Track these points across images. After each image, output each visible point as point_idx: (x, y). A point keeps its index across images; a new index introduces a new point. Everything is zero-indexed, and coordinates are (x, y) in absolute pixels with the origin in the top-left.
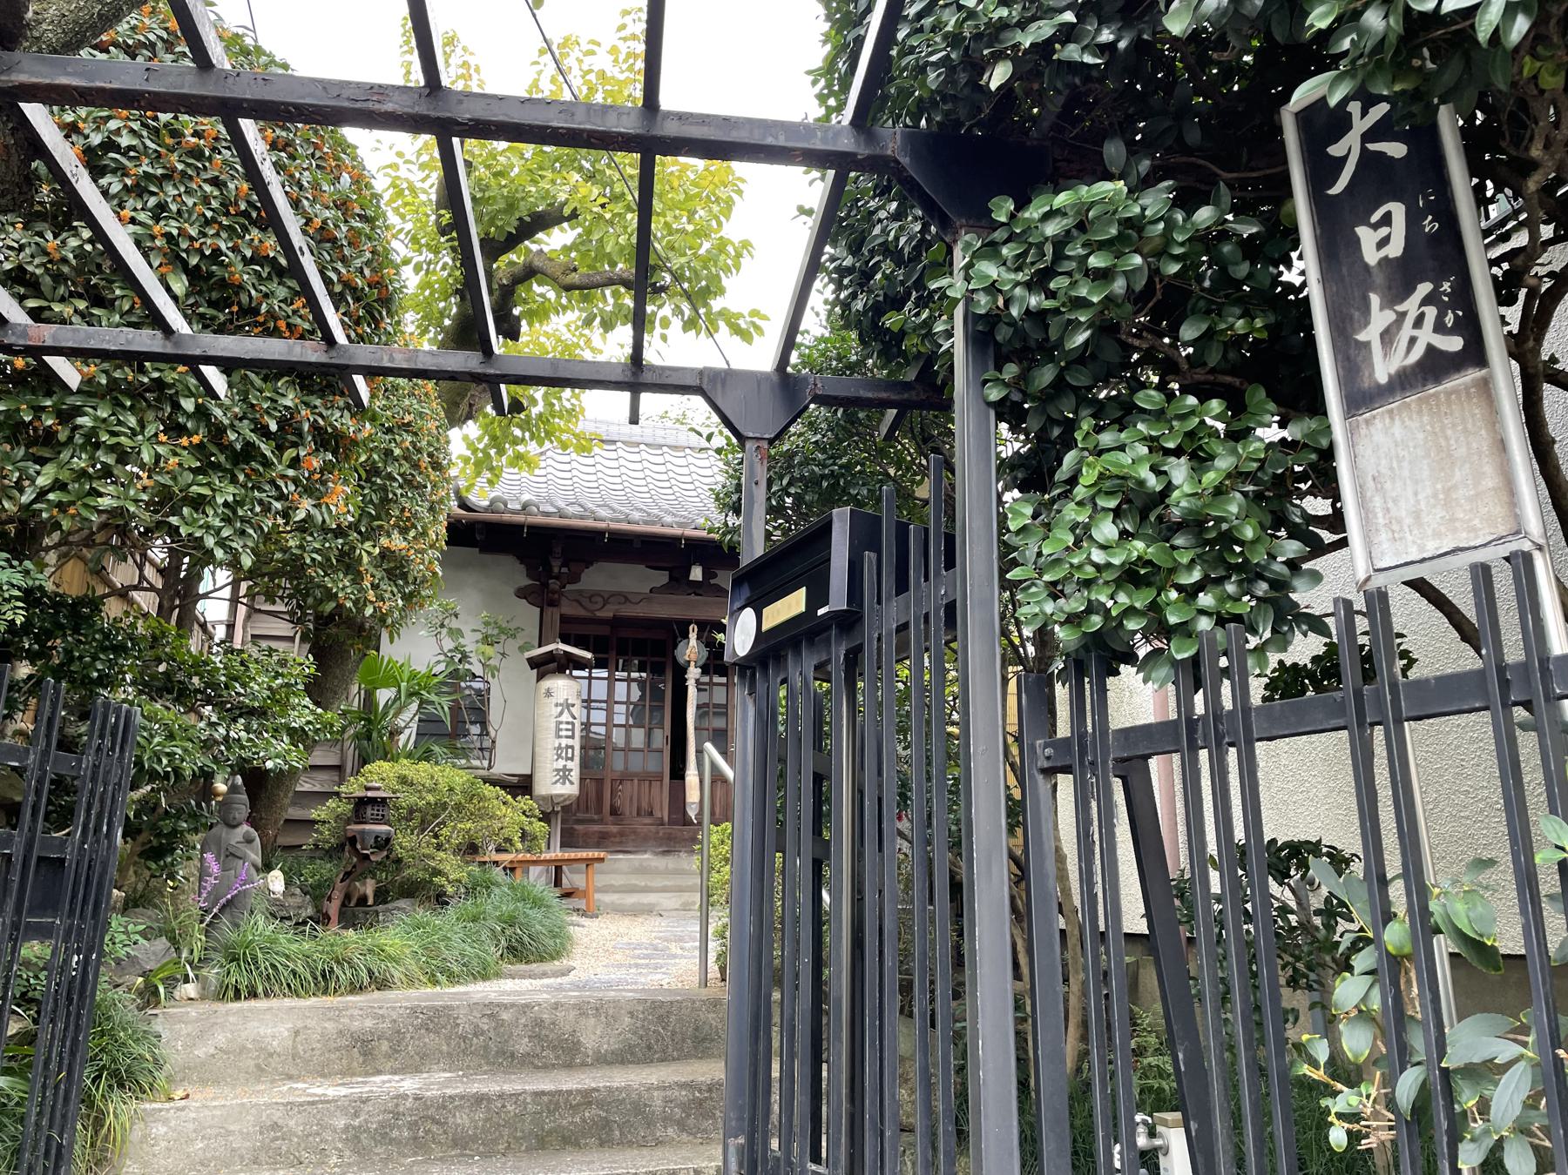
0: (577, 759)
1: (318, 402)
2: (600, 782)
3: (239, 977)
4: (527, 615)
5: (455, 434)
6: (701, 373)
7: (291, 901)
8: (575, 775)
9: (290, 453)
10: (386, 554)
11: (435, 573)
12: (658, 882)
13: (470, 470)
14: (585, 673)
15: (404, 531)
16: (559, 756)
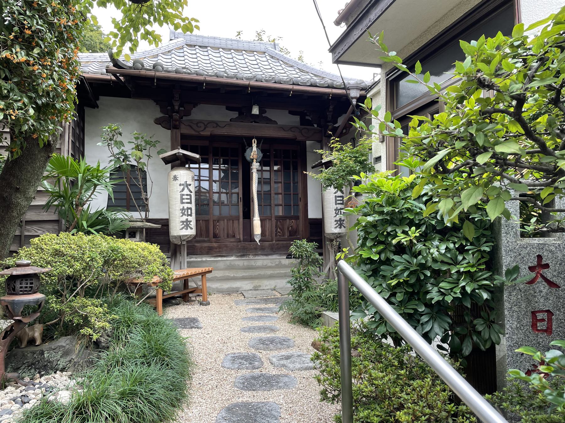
0: (194, 215)
2: (207, 221)
4: (164, 135)
8: (193, 224)
12: (240, 274)
14: (197, 166)
16: (183, 214)
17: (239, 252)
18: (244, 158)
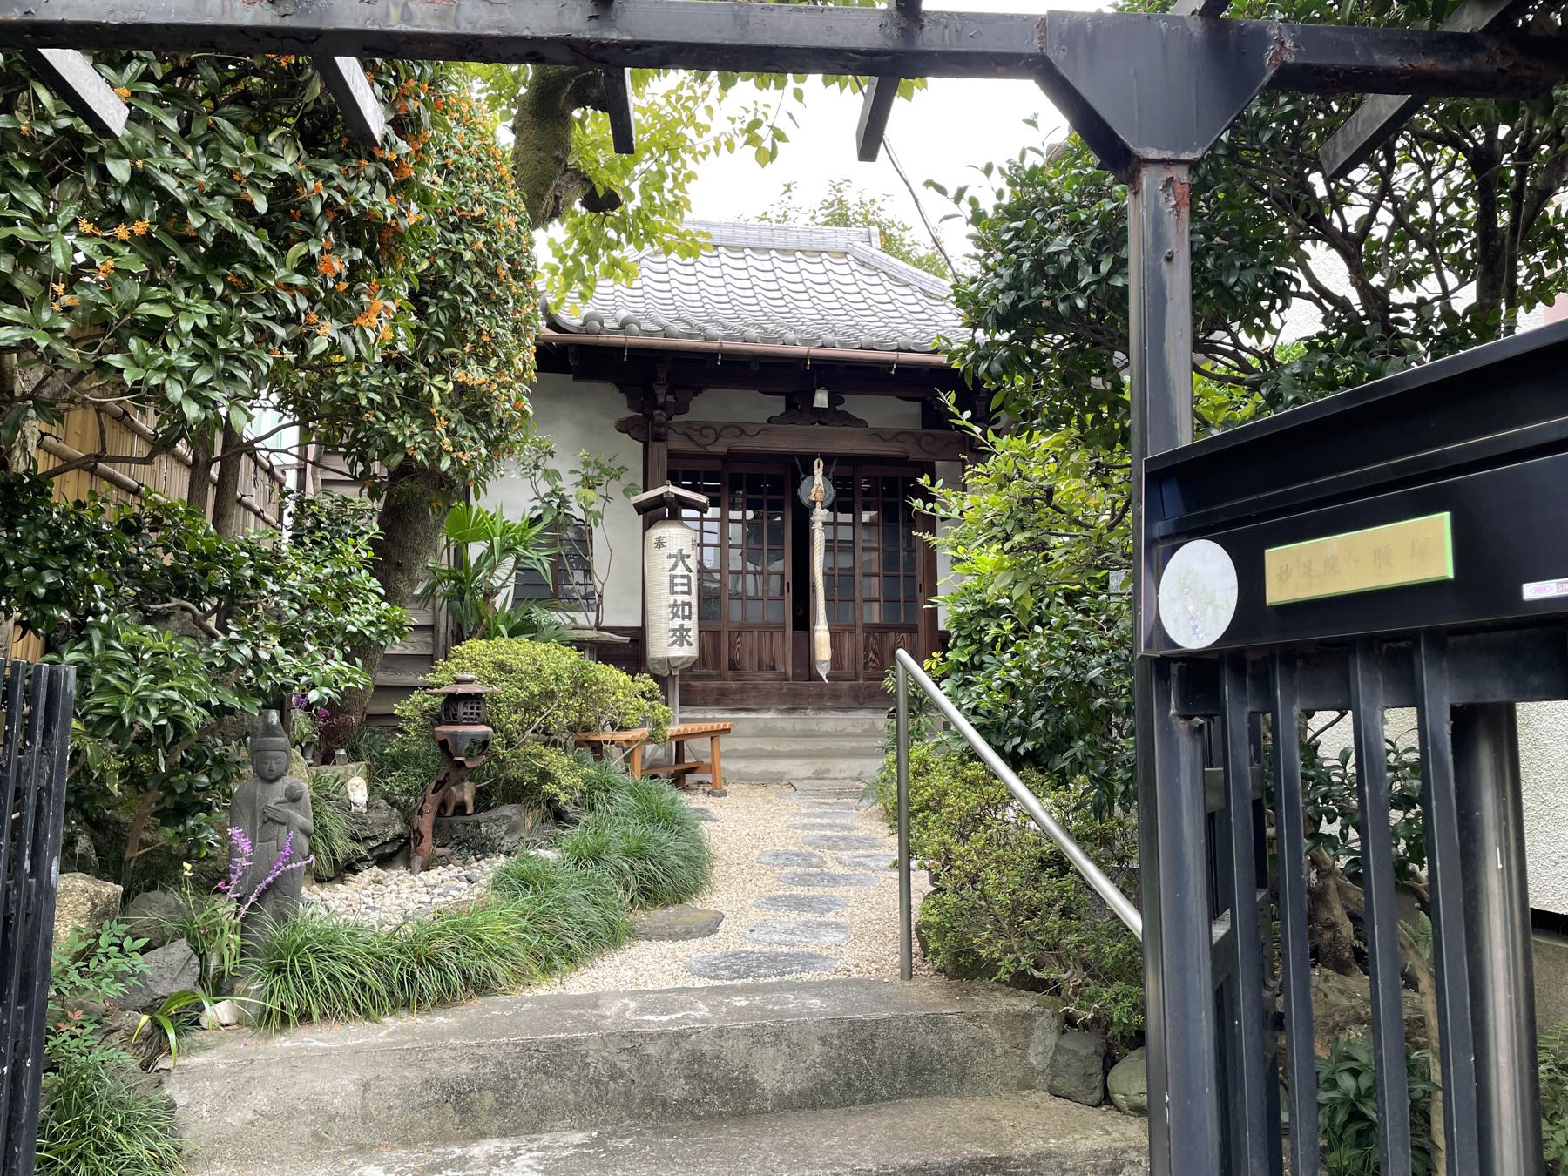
0: (695, 617)
1: (333, 168)
2: (716, 634)
3: (286, 997)
4: (630, 451)
5: (539, 235)
6: (1047, 24)
7: (375, 816)
8: (693, 636)
9: (298, 250)
10: (461, 388)
11: (524, 413)
12: (786, 746)
13: (559, 281)
15: (483, 361)
16: (675, 615)
17: (785, 703)
18: (797, 502)
